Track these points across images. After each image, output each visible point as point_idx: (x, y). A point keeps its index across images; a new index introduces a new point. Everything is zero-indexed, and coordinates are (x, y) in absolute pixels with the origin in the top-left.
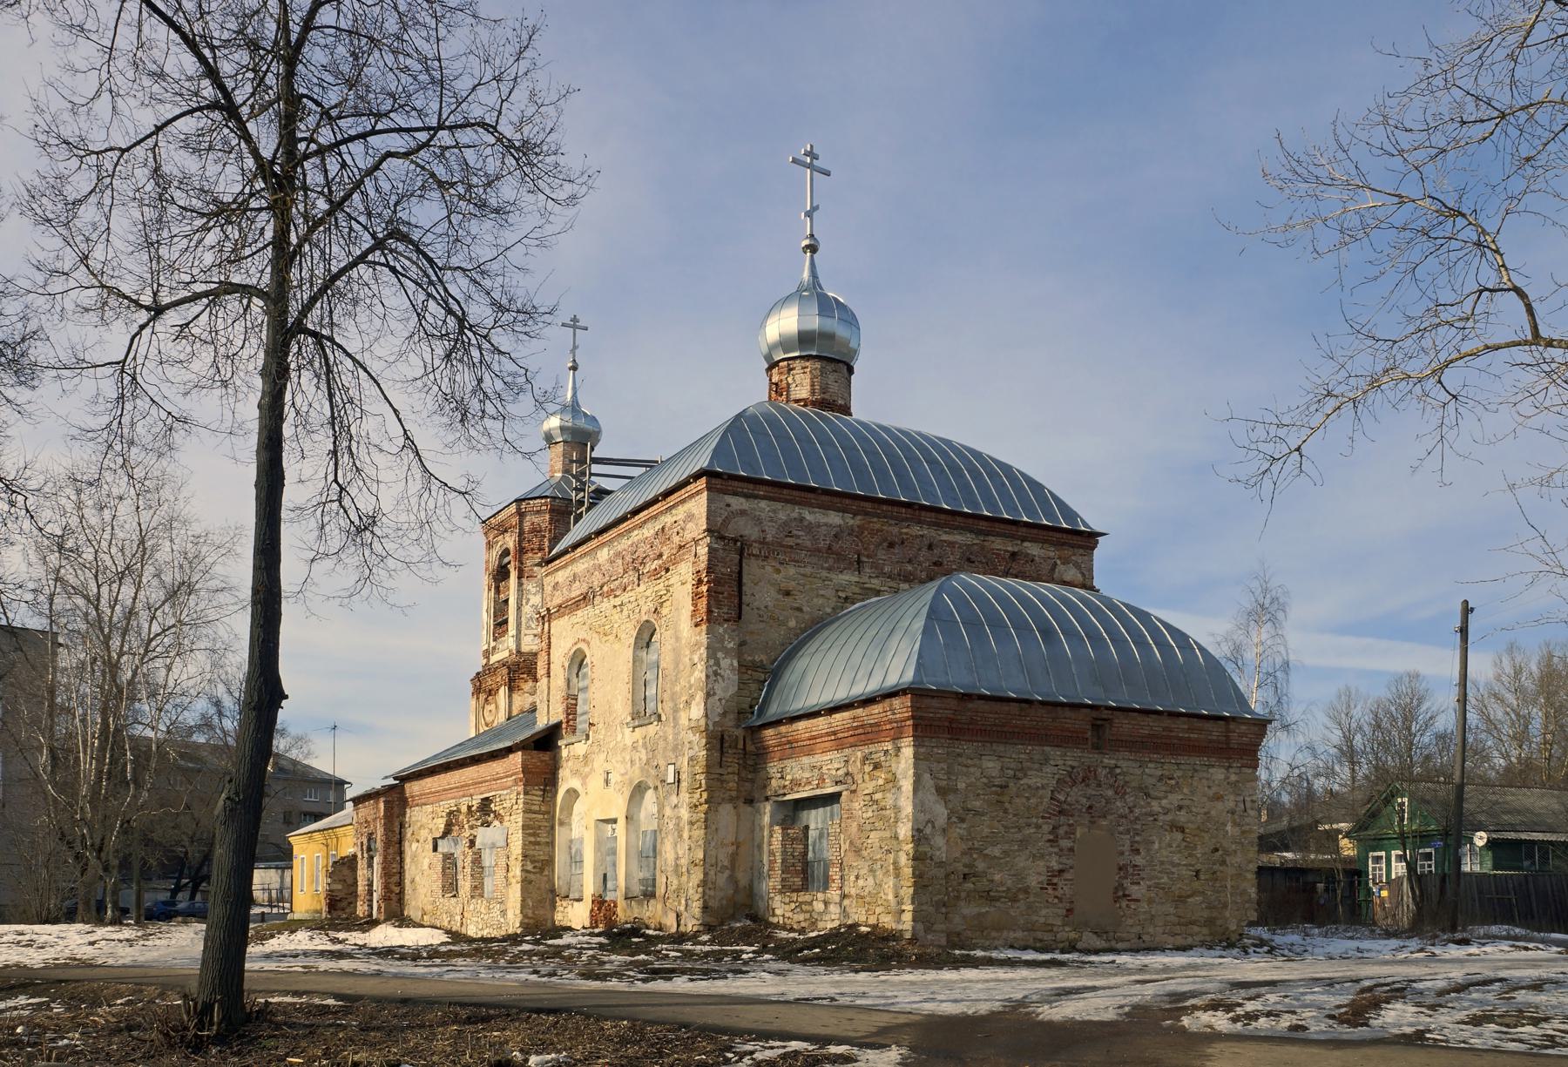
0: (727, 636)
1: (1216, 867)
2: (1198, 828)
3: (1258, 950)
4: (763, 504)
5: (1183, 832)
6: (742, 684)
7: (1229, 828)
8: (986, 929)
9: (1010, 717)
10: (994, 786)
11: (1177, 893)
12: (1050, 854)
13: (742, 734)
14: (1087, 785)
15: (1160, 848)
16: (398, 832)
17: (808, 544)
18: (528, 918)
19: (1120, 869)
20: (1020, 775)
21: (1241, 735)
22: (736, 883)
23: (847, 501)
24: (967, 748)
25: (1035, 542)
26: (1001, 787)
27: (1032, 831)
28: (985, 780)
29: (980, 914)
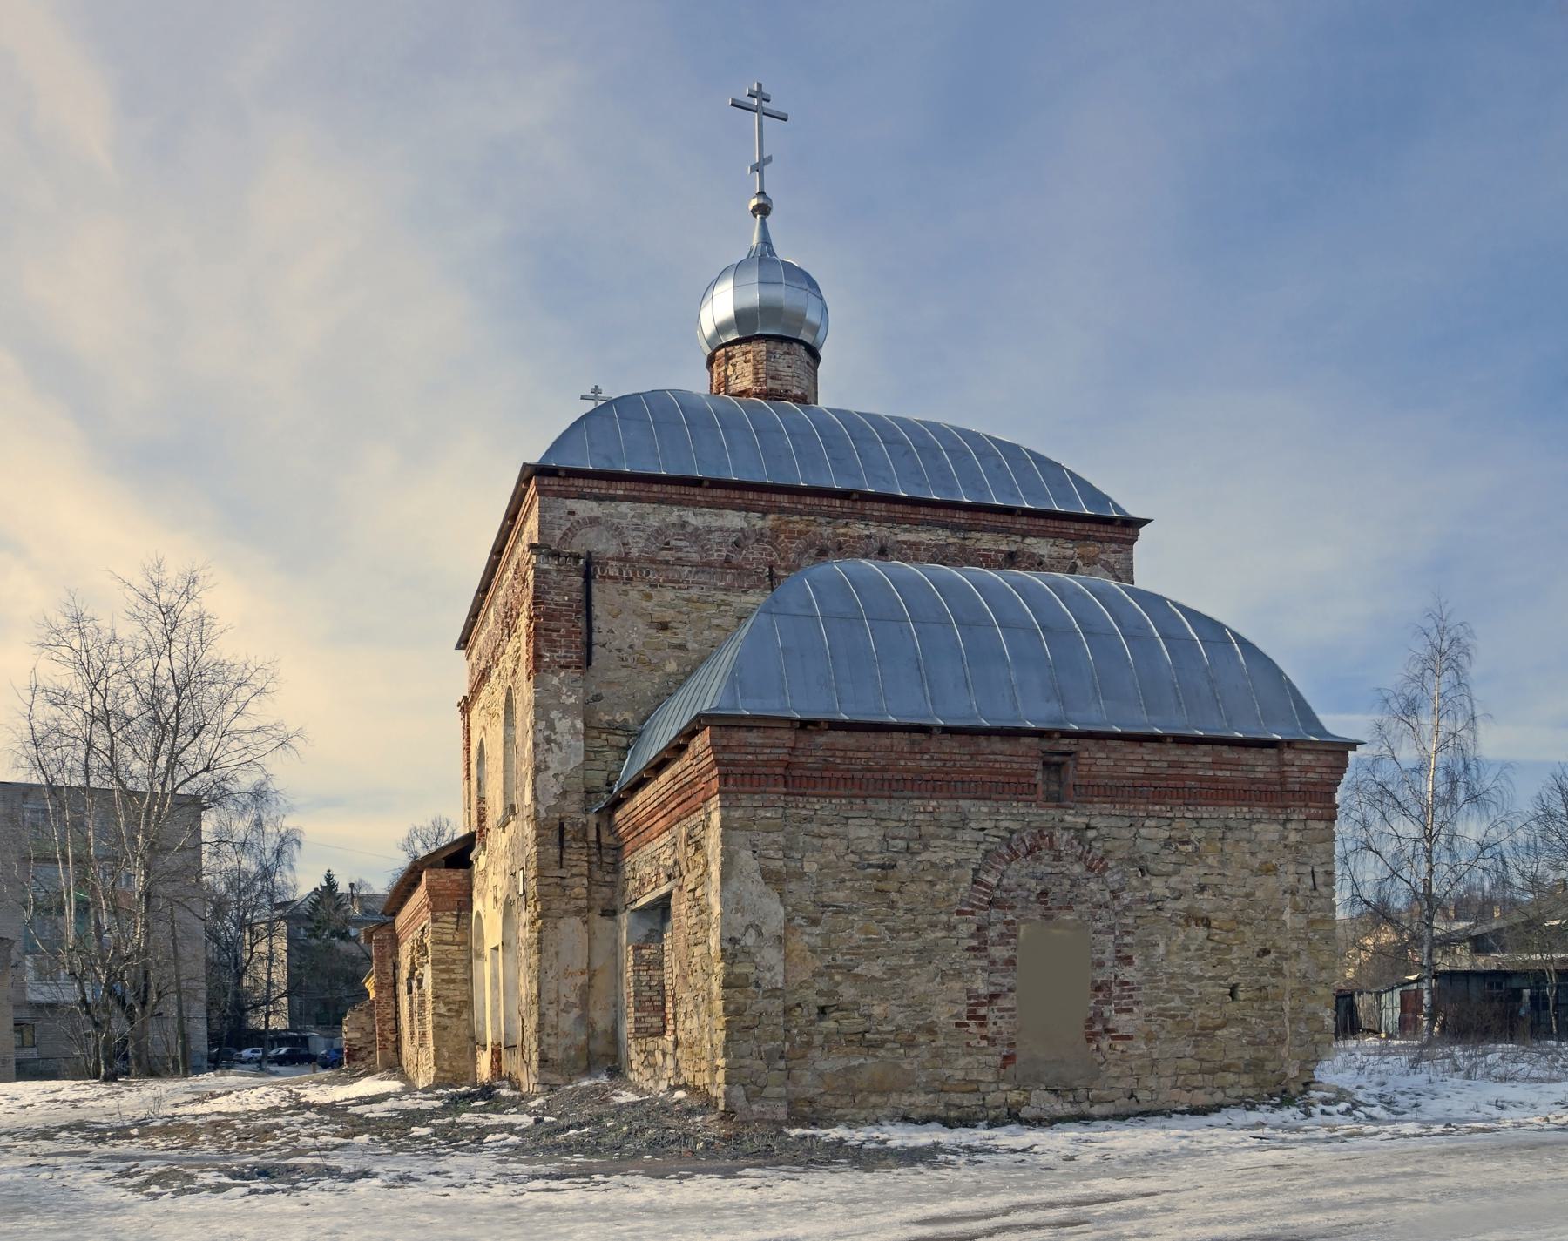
0: (564, 688)
2: (1234, 918)
3: (1328, 1108)
4: (624, 507)
5: (1208, 925)
6: (591, 754)
7: (1286, 916)
8: (861, 1091)
9: (893, 755)
10: (870, 866)
11: (1197, 1022)
12: (973, 970)
13: (595, 821)
14: (1039, 859)
15: (1168, 953)
16: (391, 973)
17: (695, 557)
18: (444, 1071)
19: (1098, 989)
20: (915, 846)
21: (1305, 769)
22: (591, 1025)
23: (751, 495)
24: (822, 808)
25: (1043, 537)
26: (882, 867)
27: (939, 935)
28: (853, 858)
29: (847, 1069)
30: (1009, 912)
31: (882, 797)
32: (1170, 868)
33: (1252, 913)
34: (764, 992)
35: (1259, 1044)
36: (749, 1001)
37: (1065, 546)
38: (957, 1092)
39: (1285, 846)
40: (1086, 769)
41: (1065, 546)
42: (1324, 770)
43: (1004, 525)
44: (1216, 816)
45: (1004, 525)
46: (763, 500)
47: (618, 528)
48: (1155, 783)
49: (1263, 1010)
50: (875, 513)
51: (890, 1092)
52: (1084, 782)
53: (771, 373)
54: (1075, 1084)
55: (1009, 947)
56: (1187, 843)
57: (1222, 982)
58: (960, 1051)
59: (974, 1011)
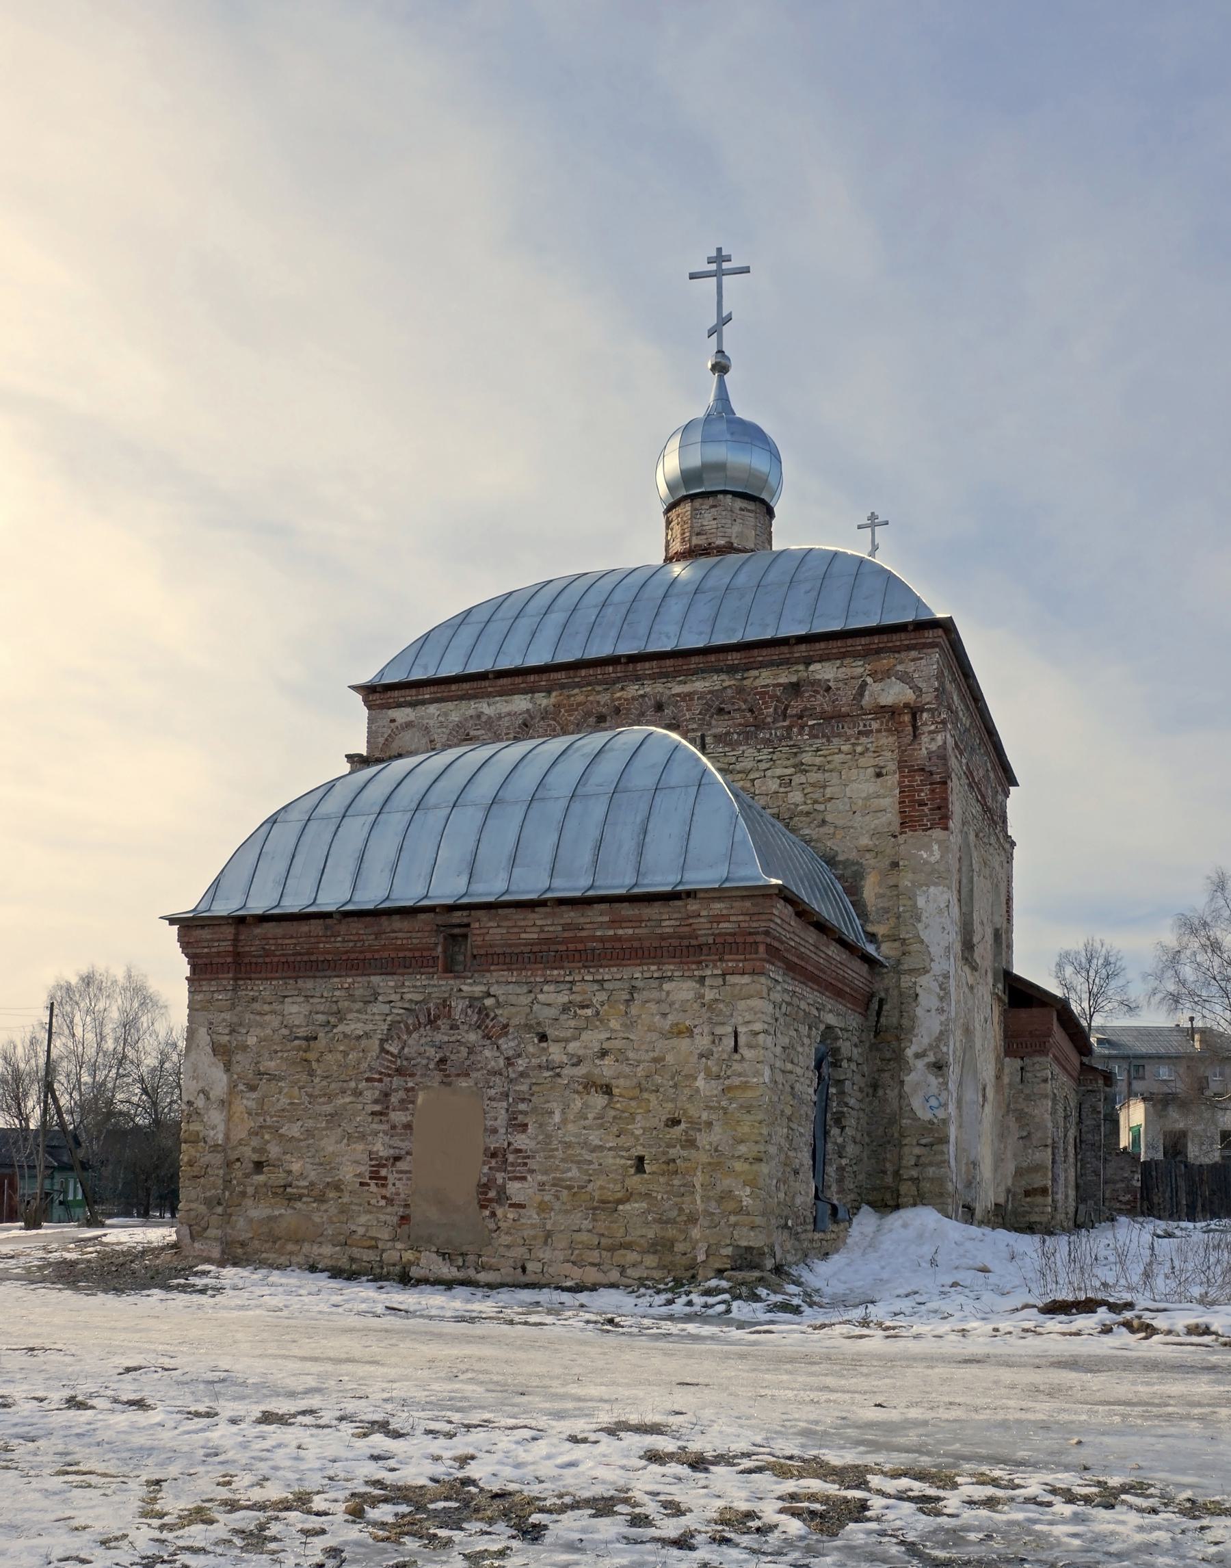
1: (673, 1152)
4: (432, 709)
7: (700, 1083)
8: (280, 1239)
9: (313, 940)
10: (297, 1038)
11: (596, 1195)
12: (376, 1133)
15: (564, 1121)
20: (333, 1020)
21: (717, 919)
24: (264, 988)
25: (828, 660)
26: (307, 1039)
27: (348, 1100)
29: (271, 1219)
30: (409, 1079)
31: (309, 977)
32: (569, 1034)
33: (658, 1079)
34: (210, 1147)
35: (667, 1222)
36: (198, 1155)
37: (854, 664)
38: (358, 1247)
39: (703, 1005)
40: (480, 939)
41: (854, 664)
42: (741, 918)
43: (781, 657)
44: (619, 976)
45: (781, 657)
46: (543, 681)
47: (427, 728)
48: (553, 948)
49: (673, 1186)
50: (647, 672)
51: (303, 1241)
52: (482, 952)
53: (697, 530)
54: (464, 1249)
55: (408, 1113)
56: (587, 1007)
57: (624, 1153)
58: (361, 1209)
59: (377, 1172)
